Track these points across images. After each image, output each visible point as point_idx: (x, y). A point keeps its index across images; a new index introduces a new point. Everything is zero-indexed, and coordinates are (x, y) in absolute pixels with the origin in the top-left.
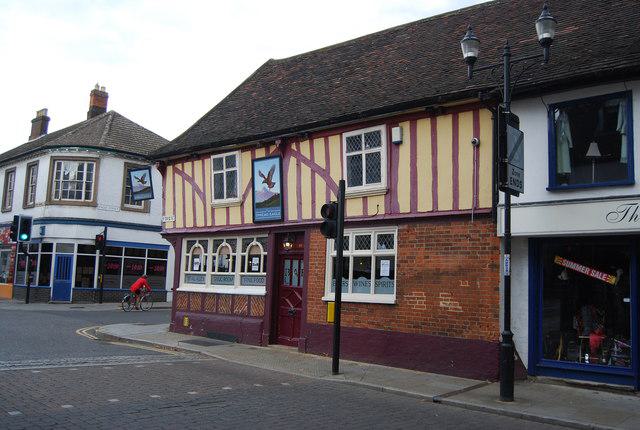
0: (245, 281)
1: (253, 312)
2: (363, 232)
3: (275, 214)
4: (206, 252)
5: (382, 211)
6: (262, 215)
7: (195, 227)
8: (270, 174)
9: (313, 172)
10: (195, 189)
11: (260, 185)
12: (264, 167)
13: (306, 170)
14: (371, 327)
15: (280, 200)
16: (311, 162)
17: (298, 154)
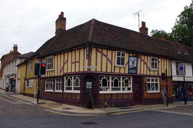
0: (75, 89)
1: (129, 97)
2: (156, 78)
3: (134, 72)
4: (72, 80)
5: (157, 75)
6: (131, 71)
7: (111, 72)
8: (134, 61)
9: (144, 63)
10: (108, 59)
11: (131, 63)
12: (133, 59)
13: (142, 63)
14: (156, 97)
15: (136, 68)
16: (144, 61)
17: (141, 58)
